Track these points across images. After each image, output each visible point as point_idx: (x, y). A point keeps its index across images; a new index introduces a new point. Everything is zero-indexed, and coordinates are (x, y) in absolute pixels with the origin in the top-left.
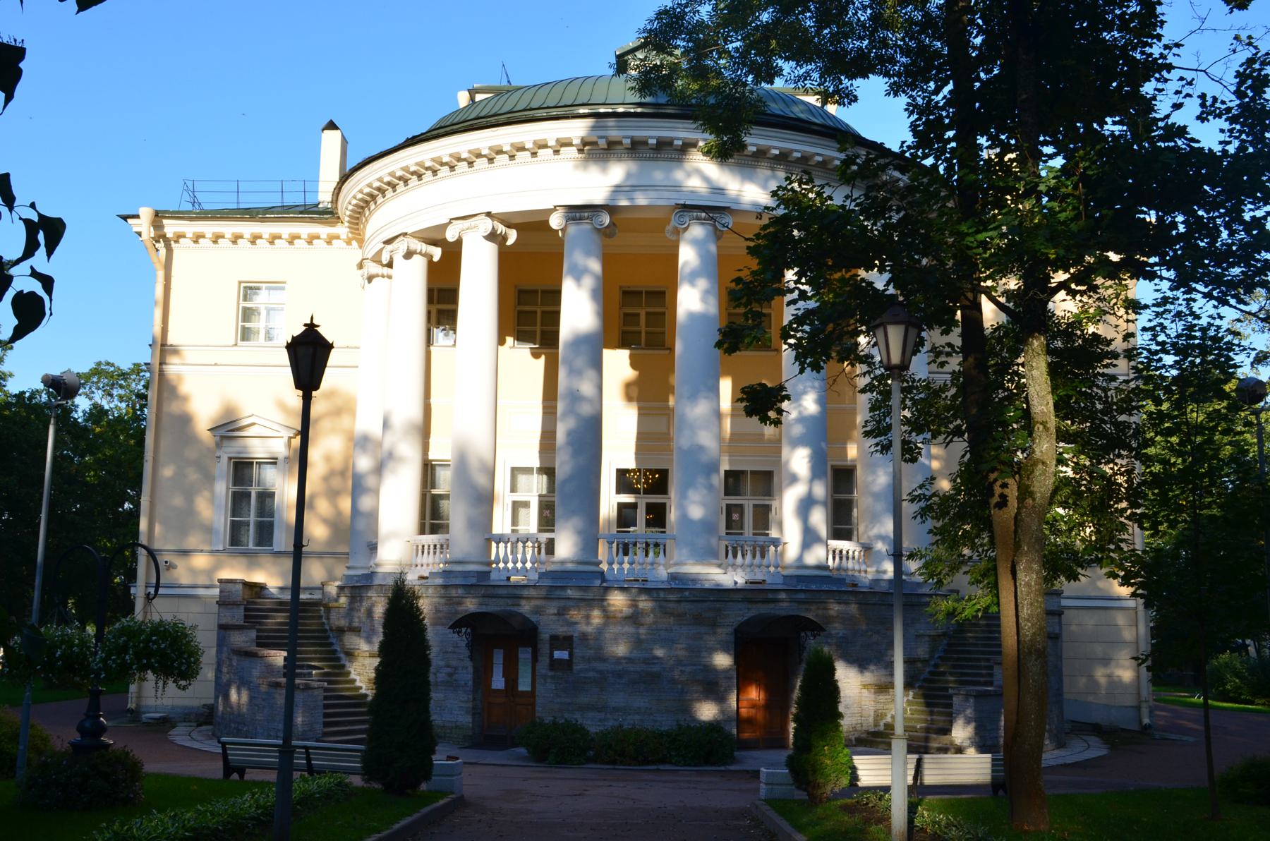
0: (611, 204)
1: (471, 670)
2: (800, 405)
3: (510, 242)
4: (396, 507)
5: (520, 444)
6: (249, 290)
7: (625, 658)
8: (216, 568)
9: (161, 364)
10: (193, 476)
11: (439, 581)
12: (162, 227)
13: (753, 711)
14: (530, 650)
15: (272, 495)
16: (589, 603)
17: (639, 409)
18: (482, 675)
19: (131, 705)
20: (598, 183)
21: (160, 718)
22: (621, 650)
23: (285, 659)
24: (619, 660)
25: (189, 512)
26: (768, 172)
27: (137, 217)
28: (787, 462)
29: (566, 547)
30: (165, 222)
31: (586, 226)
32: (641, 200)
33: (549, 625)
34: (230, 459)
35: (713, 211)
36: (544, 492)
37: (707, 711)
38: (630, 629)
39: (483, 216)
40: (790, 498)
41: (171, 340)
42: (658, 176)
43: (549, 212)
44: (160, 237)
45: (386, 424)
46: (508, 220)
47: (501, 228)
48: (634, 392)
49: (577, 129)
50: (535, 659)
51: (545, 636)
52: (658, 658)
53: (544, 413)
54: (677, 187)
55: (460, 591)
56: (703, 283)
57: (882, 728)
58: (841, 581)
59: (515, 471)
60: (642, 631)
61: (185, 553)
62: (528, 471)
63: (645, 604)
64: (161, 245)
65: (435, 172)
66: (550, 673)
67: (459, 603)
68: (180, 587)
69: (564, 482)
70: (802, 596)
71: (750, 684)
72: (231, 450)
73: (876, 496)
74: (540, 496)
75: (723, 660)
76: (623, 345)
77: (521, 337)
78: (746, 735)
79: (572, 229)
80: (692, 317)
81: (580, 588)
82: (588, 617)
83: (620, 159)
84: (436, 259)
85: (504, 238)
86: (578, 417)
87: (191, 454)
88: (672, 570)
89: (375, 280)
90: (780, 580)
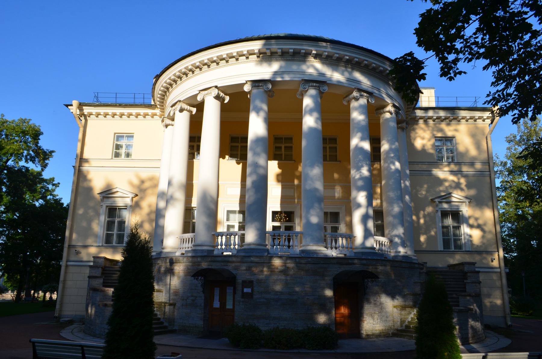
0: (272, 80)
1: (203, 298)
2: (361, 172)
3: (226, 102)
4: (173, 221)
5: (230, 200)
6: (119, 137)
7: (280, 292)
8: (100, 252)
9: (79, 167)
10: (91, 213)
11: (190, 255)
12: (83, 110)
13: (342, 319)
14: (232, 288)
15: (124, 222)
16: (262, 264)
17: (282, 186)
18: (209, 300)
19: (56, 314)
20: (266, 71)
21: (68, 321)
22: (278, 288)
23: (113, 292)
24: (276, 293)
25: (89, 228)
26: (343, 69)
27: (72, 105)
28: (355, 198)
29: (251, 237)
30: (84, 107)
31: (261, 90)
32: (287, 78)
33: (242, 274)
34: (107, 206)
35: (320, 83)
36: (241, 221)
37: (322, 319)
38: (283, 277)
39: (214, 88)
40: (357, 216)
41: (85, 156)
42: (294, 67)
43: (243, 85)
44: (82, 114)
45: (170, 183)
46: (224, 89)
47: (222, 94)
48: (280, 178)
49: (257, 46)
50: (235, 293)
51: (239, 280)
52: (296, 292)
53: (241, 188)
54: (303, 73)
55: (199, 259)
56: (316, 115)
57: (404, 328)
58: (382, 255)
59: (229, 212)
60: (288, 278)
61: (86, 247)
62: (234, 212)
63: (291, 265)
64: (83, 118)
65: (193, 72)
66: (242, 300)
67: (199, 265)
68: (82, 261)
69: (250, 206)
70: (365, 262)
71: (341, 306)
72: (108, 202)
73: (394, 217)
74: (240, 223)
75: (329, 293)
76: (275, 159)
77: (232, 156)
78: (340, 331)
79: (255, 91)
80: (311, 129)
81: (257, 257)
82: (262, 271)
83: (277, 60)
84: (194, 113)
85: (224, 99)
86: (258, 174)
87: (91, 204)
88: (301, 249)
89: (169, 127)
90: (353, 255)
